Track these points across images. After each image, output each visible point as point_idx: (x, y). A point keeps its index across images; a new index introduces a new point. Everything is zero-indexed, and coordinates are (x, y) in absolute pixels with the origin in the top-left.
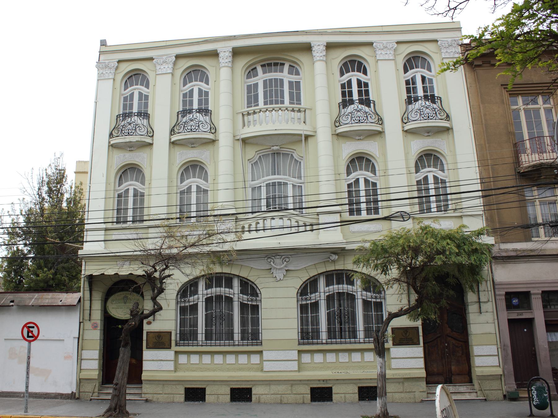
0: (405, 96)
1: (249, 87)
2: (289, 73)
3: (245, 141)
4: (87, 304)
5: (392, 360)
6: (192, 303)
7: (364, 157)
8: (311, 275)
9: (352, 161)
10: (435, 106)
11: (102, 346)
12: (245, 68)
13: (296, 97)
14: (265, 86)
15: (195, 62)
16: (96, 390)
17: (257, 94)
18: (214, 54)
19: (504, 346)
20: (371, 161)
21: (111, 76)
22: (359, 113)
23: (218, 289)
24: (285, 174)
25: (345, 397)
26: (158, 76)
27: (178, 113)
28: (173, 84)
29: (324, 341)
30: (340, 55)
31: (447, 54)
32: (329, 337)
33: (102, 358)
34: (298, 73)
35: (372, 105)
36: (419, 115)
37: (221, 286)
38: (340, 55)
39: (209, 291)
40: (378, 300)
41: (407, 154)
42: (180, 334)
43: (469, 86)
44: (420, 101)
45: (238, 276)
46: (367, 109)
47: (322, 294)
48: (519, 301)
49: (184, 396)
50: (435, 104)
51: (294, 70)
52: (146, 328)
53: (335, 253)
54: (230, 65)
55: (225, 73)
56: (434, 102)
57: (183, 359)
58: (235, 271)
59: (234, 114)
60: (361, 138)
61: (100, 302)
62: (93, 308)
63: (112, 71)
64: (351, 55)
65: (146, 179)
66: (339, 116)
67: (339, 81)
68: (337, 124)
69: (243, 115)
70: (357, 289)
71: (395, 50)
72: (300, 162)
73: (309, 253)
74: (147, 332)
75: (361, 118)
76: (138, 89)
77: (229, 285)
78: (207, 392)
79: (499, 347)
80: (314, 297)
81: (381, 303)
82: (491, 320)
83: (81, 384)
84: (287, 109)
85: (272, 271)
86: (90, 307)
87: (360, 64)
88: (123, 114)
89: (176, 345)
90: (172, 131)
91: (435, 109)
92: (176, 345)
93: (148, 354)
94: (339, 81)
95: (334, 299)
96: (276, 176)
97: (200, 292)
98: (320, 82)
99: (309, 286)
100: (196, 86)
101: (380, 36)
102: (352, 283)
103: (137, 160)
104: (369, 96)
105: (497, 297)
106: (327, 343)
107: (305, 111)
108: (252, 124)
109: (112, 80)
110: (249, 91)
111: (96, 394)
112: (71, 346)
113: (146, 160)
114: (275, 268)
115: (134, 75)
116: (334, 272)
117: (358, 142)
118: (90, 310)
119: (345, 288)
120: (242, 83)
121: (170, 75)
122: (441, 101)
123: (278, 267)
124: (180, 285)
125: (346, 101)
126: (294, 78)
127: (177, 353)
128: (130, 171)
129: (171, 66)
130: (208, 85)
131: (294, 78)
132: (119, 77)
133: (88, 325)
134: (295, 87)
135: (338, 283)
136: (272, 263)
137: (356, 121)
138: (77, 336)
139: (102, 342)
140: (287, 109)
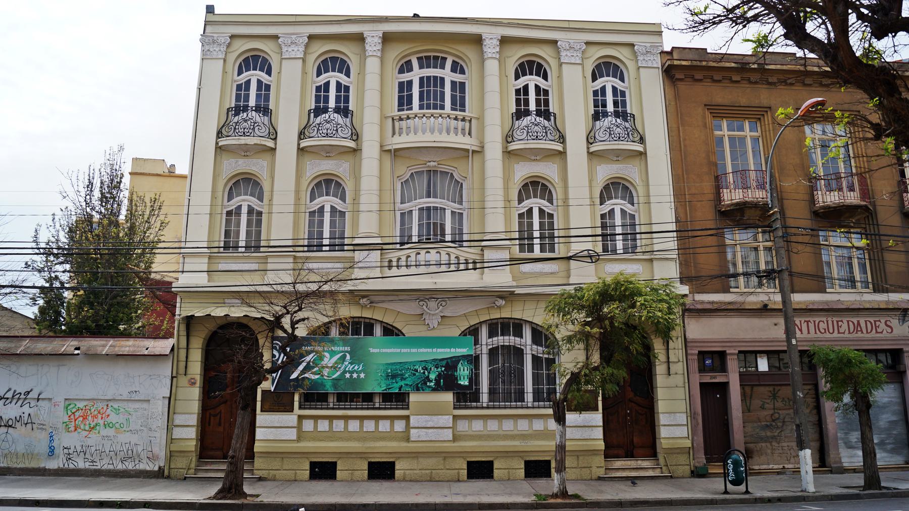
4: (183, 353)
10: (627, 125)
13: (459, 103)
14: (421, 85)
16: (193, 465)
30: (516, 55)
35: (552, 118)
40: (551, 357)
47: (484, 347)
53: (501, 297)
56: (626, 120)
59: (383, 118)
60: (538, 158)
62: (190, 358)
64: (531, 52)
69: (393, 119)
86: (187, 357)
89: (300, 408)
90: (302, 135)
91: (546, 128)
92: (300, 408)
93: (262, 418)
94: (514, 86)
96: (431, 200)
98: (493, 88)
105: (689, 357)
111: (192, 471)
119: (510, 340)
120: (395, 79)
126: (458, 78)
127: (301, 418)
129: (302, 49)
131: (458, 78)
132: (232, 57)
133: (183, 381)
134: (459, 88)
135: (502, 335)
136: (424, 307)
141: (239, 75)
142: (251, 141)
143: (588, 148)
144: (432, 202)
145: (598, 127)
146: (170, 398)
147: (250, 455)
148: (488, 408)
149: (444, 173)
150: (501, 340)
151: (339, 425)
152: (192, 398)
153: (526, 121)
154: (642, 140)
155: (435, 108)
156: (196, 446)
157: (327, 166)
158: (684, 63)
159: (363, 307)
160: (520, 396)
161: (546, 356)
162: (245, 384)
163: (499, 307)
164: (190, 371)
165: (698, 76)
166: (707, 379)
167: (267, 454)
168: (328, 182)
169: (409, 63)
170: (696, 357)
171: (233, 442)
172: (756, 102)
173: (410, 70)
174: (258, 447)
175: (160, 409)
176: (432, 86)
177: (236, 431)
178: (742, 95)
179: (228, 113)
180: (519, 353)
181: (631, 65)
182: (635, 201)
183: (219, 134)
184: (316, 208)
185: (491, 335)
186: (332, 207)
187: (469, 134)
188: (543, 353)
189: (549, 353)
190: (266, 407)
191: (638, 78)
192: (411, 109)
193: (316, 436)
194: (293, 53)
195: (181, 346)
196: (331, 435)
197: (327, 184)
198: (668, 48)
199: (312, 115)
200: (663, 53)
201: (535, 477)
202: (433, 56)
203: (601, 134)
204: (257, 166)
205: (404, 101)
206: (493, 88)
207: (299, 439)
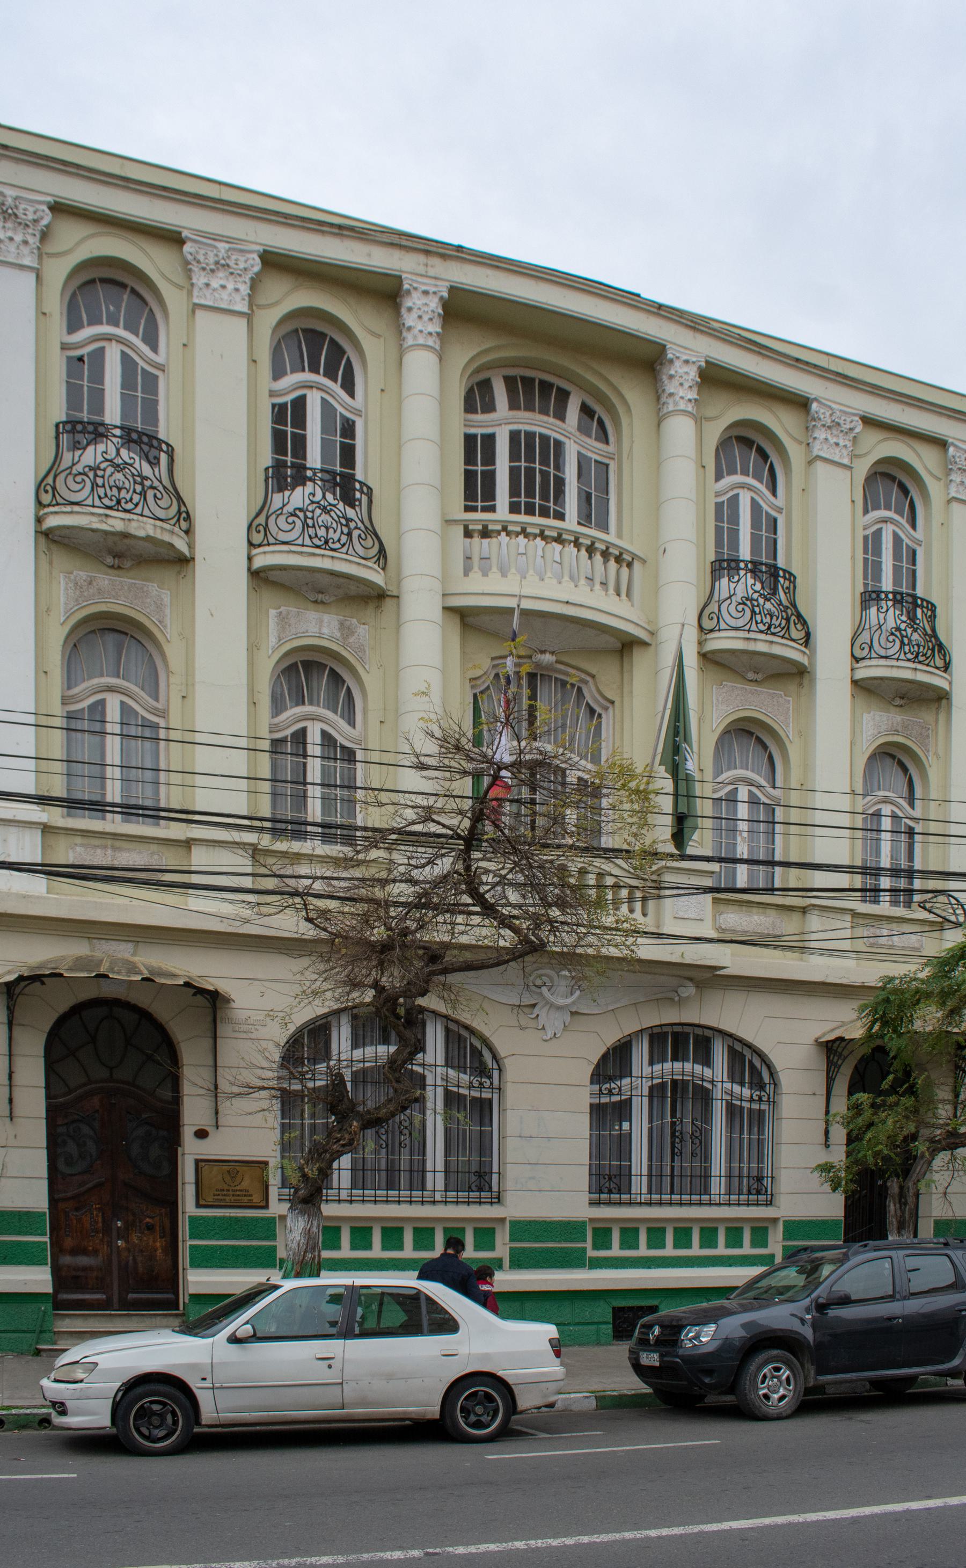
0: (266, 458)
10: (351, 513)
13: (594, 509)
20: (344, 681)
22: (119, 476)
23: (678, 1065)
26: (199, 313)
27: (57, 426)
34: (603, 437)
35: (163, 457)
37: (685, 1059)
39: (657, 1067)
40: (486, 1095)
41: (253, 648)
44: (309, 486)
46: (147, 470)
50: (352, 506)
51: (596, 421)
56: (349, 500)
60: (759, 677)
62: (18, 1079)
63: (31, 240)
66: (53, 469)
67: (272, 394)
68: (257, 538)
70: (716, 1072)
71: (45, 236)
72: (600, 716)
74: (197, 1162)
75: (123, 493)
81: (490, 1101)
84: (505, 529)
87: (337, 351)
91: (349, 520)
94: (272, 394)
99: (614, 1063)
101: (907, 409)
102: (706, 1061)
104: (353, 468)
106: (650, 1204)
107: (630, 565)
108: (476, 568)
110: (469, 457)
115: (104, 281)
122: (370, 502)
124: (292, 1028)
134: (597, 479)
135: (675, 1058)
140: (505, 529)
145: (725, 595)
150: (671, 1069)
153: (298, 497)
154: (807, 639)
155: (544, 513)
157: (319, 627)
169: (485, 386)
173: (489, 407)
176: (535, 452)
180: (704, 1096)
182: (918, 793)
184: (288, 732)
186: (324, 734)
187: (628, 595)
188: (751, 1100)
190: (256, 1199)
192: (492, 509)
205: (478, 489)
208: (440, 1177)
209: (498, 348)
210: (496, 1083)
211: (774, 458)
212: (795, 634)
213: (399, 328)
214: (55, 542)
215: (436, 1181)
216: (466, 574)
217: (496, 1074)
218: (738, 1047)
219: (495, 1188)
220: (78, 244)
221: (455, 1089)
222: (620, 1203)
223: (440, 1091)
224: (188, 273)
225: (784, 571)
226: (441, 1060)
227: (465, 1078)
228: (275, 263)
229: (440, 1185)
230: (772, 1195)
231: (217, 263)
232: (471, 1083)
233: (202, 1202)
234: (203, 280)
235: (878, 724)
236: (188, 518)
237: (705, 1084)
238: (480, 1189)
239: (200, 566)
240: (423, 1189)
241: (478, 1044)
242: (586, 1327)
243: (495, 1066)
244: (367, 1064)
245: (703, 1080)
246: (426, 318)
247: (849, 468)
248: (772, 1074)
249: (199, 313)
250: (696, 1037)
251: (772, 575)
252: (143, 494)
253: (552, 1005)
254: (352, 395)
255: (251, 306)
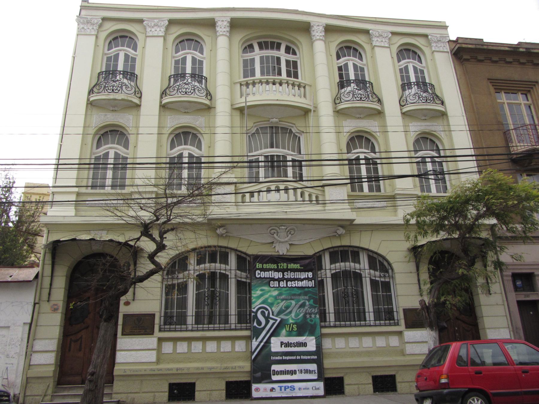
0: (337, 80)
1: (245, 62)
2: (286, 52)
3: (241, 110)
4: (47, 281)
5: (407, 345)
6: (182, 280)
7: (363, 137)
8: (317, 251)
9: (352, 139)
11: (62, 335)
12: (244, 40)
14: (262, 62)
15: (190, 30)
16: (50, 392)
17: (254, 69)
18: (211, 24)
19: (517, 328)
21: (94, 32)
23: (342, 264)
24: (284, 148)
25: (358, 388)
26: (148, 39)
28: (165, 48)
29: (332, 324)
30: (338, 39)
31: (436, 48)
32: (197, 322)
33: (60, 350)
34: (294, 53)
36: (417, 98)
37: (215, 262)
38: (338, 39)
40: (387, 280)
42: (165, 316)
43: (459, 77)
45: (236, 250)
47: (328, 271)
48: (522, 283)
49: (167, 394)
52: (123, 309)
53: (342, 227)
54: (228, 34)
55: (222, 42)
57: (167, 348)
58: (233, 244)
59: (232, 84)
60: (362, 116)
61: (65, 278)
62: (54, 285)
63: (95, 28)
64: (349, 38)
65: (130, 142)
69: (241, 85)
72: (299, 138)
73: (317, 224)
76: (124, 50)
77: (225, 260)
78: (197, 388)
79: (511, 330)
80: (181, 277)
81: (389, 282)
82: (500, 302)
83: (29, 385)
85: (274, 245)
86: (51, 285)
88: (106, 71)
89: (160, 330)
90: (163, 93)
92: (160, 330)
93: (123, 342)
94: (338, 64)
95: (351, 277)
96: (274, 149)
97: (191, 267)
98: (320, 62)
100: (189, 55)
103: (121, 121)
105: (505, 278)
107: (304, 87)
109: (94, 37)
111: (48, 398)
112: (19, 333)
113: (131, 121)
114: (278, 241)
116: (351, 249)
117: (358, 120)
118: (50, 289)
119: (350, 265)
120: (239, 57)
121: (162, 39)
123: (282, 240)
125: (343, 83)
126: (291, 57)
127: (161, 340)
128: (113, 133)
129: (163, 29)
130: (202, 54)
131: (291, 57)
132: (103, 35)
133: (46, 307)
136: (275, 235)
137: (357, 99)
138: (29, 321)
139: (62, 328)
141: (109, 50)
142: (119, 96)
143: (401, 110)
144: (275, 151)
146: (31, 324)
147: (110, 379)
148: (335, 326)
149: (284, 129)
150: (341, 266)
151: (197, 347)
152: (52, 324)
154: (443, 103)
156: (54, 371)
157: (185, 120)
158: (470, 46)
159: (220, 236)
160: (361, 316)
161: (383, 280)
162: (111, 293)
163: (340, 236)
164: (54, 297)
165: (480, 57)
166: (522, 298)
167: (126, 377)
168: (186, 134)
170: (510, 278)
171: (94, 357)
172: (526, 78)
174: (118, 370)
175: (20, 336)
177: (98, 344)
178: (514, 73)
179: (98, 77)
180: (358, 277)
181: (426, 50)
183: (91, 91)
185: (332, 261)
188: (380, 277)
189: (385, 276)
190: (128, 331)
191: (433, 59)
193: (175, 357)
194: (156, 32)
195: (45, 274)
196: (189, 357)
197: (185, 135)
198: (453, 38)
199: (172, 80)
200: (450, 41)
201: (382, 391)
202: (272, 39)
203: (411, 97)
204: (124, 119)
206: (320, 62)
207: (158, 361)
208: (372, 315)
209: (251, 34)
210: (390, 274)
211: (419, 52)
212: (437, 102)
213: (216, 32)
214: (94, 106)
215: (370, 316)
216: (241, 97)
217: (390, 271)
218: (371, 254)
219: (396, 318)
220: (111, 27)
221: (374, 278)
222: (360, 326)
223: (368, 280)
224: (145, 29)
225: (429, 84)
226: (367, 267)
227: (377, 273)
228: (172, 22)
229: (372, 318)
230: (398, 320)
231: (154, 25)
232: (380, 275)
233: (124, 333)
234: (150, 29)
235: (416, 127)
236: (210, 95)
237: (357, 271)
238: (390, 320)
239: (142, 108)
240: (365, 320)
241: (381, 260)
242: (146, 394)
243: (389, 268)
244: (337, 271)
245: (355, 269)
246: (223, 27)
247: (389, 47)
248: (389, 264)
249: (376, 48)
250: (351, 251)
251: (422, 84)
252: (194, 90)
253: (280, 242)
254: (421, 63)
255: (165, 34)
